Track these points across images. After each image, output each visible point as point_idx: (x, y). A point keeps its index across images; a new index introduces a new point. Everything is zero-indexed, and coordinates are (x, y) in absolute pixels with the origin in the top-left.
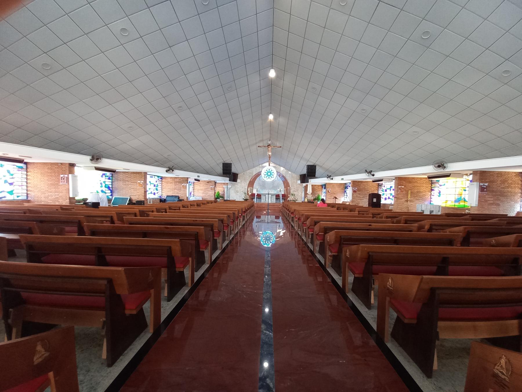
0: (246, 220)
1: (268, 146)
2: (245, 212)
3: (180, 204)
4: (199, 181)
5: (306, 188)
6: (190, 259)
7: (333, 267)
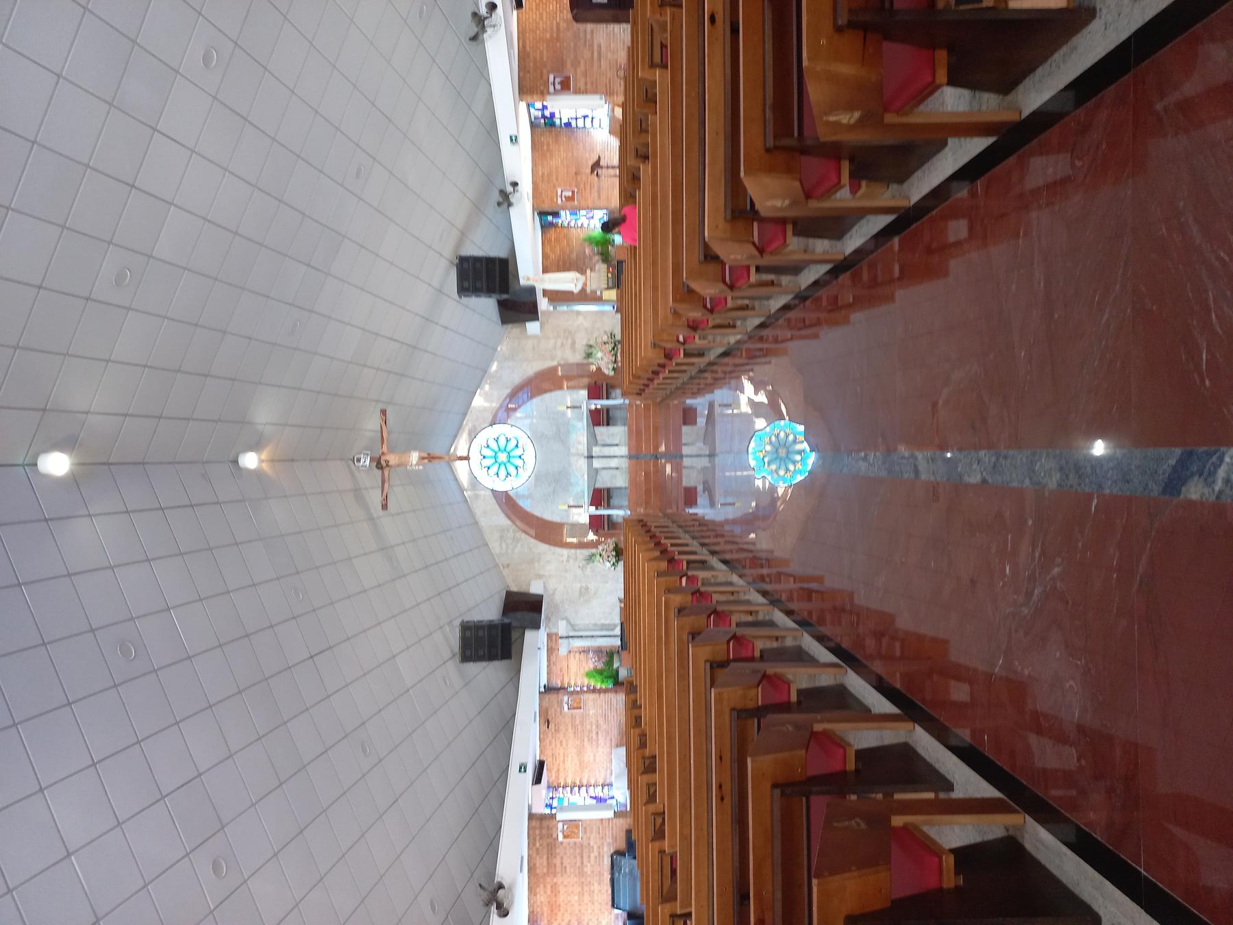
0: (703, 555)
1: (379, 466)
2: (671, 561)
3: (648, 850)
4: (541, 764)
5: (556, 297)
6: (898, 821)
7: (902, 177)
